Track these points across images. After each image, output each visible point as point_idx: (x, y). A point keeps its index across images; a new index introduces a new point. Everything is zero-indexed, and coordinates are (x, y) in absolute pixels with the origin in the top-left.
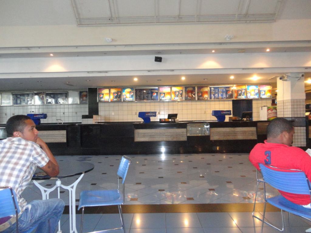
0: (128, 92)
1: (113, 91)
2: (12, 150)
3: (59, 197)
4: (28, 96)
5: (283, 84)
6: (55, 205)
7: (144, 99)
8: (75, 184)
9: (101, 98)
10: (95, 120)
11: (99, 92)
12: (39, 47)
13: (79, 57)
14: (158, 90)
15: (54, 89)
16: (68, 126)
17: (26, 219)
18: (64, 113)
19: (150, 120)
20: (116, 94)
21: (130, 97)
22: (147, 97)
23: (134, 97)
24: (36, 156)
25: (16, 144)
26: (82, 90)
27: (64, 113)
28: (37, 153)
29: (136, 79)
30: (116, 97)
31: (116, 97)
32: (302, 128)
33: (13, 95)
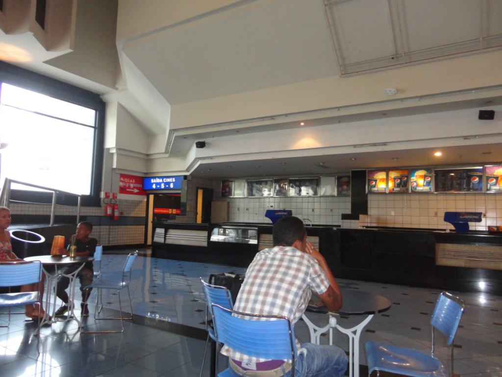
0: (421, 177)
1: (393, 175)
2: (285, 264)
3: (331, 343)
4: (266, 185)
6: (336, 357)
7: (452, 188)
8: (360, 328)
9: (371, 187)
10: (361, 223)
11: (369, 176)
12: (286, 115)
13: (340, 124)
14: (484, 170)
15: (304, 171)
16: (322, 230)
17: (301, 369)
18: (313, 210)
19: (469, 228)
20: (399, 181)
21: (424, 186)
22: (457, 184)
23: (432, 186)
24: (314, 276)
25: (289, 255)
26: (340, 175)
27: (313, 210)
28: (316, 272)
29: (438, 154)
30: (399, 185)
31: (399, 185)
32: (142, 227)
33: (248, 182)
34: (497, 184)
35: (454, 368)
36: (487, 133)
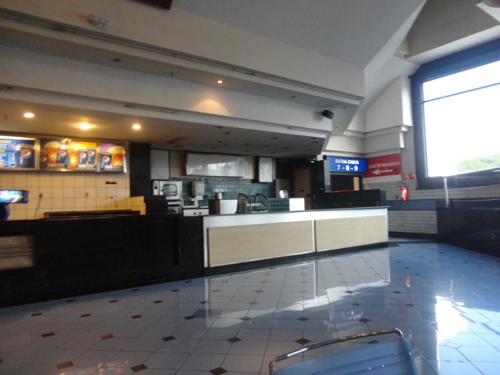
5: (158, 149)
34: (111, 163)
35: (323, 340)
36: (112, 98)
